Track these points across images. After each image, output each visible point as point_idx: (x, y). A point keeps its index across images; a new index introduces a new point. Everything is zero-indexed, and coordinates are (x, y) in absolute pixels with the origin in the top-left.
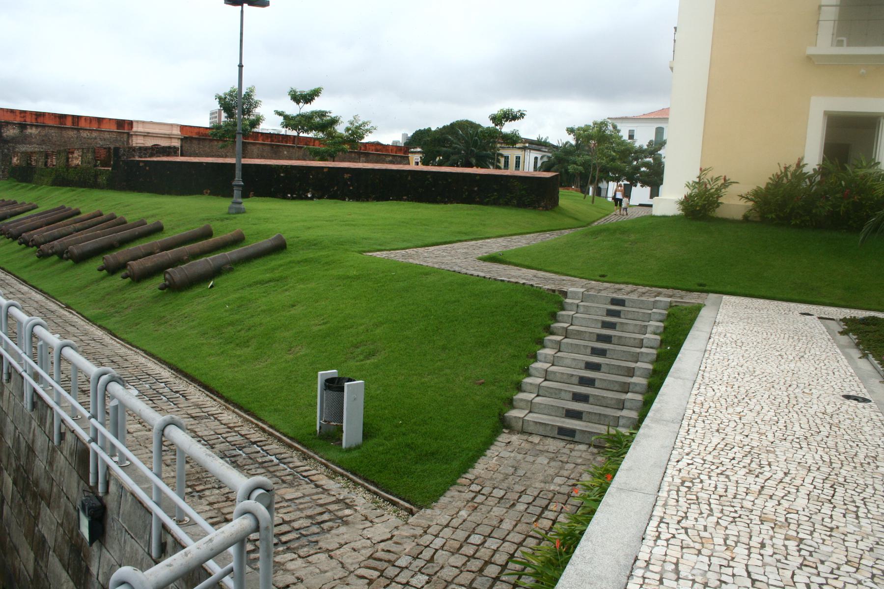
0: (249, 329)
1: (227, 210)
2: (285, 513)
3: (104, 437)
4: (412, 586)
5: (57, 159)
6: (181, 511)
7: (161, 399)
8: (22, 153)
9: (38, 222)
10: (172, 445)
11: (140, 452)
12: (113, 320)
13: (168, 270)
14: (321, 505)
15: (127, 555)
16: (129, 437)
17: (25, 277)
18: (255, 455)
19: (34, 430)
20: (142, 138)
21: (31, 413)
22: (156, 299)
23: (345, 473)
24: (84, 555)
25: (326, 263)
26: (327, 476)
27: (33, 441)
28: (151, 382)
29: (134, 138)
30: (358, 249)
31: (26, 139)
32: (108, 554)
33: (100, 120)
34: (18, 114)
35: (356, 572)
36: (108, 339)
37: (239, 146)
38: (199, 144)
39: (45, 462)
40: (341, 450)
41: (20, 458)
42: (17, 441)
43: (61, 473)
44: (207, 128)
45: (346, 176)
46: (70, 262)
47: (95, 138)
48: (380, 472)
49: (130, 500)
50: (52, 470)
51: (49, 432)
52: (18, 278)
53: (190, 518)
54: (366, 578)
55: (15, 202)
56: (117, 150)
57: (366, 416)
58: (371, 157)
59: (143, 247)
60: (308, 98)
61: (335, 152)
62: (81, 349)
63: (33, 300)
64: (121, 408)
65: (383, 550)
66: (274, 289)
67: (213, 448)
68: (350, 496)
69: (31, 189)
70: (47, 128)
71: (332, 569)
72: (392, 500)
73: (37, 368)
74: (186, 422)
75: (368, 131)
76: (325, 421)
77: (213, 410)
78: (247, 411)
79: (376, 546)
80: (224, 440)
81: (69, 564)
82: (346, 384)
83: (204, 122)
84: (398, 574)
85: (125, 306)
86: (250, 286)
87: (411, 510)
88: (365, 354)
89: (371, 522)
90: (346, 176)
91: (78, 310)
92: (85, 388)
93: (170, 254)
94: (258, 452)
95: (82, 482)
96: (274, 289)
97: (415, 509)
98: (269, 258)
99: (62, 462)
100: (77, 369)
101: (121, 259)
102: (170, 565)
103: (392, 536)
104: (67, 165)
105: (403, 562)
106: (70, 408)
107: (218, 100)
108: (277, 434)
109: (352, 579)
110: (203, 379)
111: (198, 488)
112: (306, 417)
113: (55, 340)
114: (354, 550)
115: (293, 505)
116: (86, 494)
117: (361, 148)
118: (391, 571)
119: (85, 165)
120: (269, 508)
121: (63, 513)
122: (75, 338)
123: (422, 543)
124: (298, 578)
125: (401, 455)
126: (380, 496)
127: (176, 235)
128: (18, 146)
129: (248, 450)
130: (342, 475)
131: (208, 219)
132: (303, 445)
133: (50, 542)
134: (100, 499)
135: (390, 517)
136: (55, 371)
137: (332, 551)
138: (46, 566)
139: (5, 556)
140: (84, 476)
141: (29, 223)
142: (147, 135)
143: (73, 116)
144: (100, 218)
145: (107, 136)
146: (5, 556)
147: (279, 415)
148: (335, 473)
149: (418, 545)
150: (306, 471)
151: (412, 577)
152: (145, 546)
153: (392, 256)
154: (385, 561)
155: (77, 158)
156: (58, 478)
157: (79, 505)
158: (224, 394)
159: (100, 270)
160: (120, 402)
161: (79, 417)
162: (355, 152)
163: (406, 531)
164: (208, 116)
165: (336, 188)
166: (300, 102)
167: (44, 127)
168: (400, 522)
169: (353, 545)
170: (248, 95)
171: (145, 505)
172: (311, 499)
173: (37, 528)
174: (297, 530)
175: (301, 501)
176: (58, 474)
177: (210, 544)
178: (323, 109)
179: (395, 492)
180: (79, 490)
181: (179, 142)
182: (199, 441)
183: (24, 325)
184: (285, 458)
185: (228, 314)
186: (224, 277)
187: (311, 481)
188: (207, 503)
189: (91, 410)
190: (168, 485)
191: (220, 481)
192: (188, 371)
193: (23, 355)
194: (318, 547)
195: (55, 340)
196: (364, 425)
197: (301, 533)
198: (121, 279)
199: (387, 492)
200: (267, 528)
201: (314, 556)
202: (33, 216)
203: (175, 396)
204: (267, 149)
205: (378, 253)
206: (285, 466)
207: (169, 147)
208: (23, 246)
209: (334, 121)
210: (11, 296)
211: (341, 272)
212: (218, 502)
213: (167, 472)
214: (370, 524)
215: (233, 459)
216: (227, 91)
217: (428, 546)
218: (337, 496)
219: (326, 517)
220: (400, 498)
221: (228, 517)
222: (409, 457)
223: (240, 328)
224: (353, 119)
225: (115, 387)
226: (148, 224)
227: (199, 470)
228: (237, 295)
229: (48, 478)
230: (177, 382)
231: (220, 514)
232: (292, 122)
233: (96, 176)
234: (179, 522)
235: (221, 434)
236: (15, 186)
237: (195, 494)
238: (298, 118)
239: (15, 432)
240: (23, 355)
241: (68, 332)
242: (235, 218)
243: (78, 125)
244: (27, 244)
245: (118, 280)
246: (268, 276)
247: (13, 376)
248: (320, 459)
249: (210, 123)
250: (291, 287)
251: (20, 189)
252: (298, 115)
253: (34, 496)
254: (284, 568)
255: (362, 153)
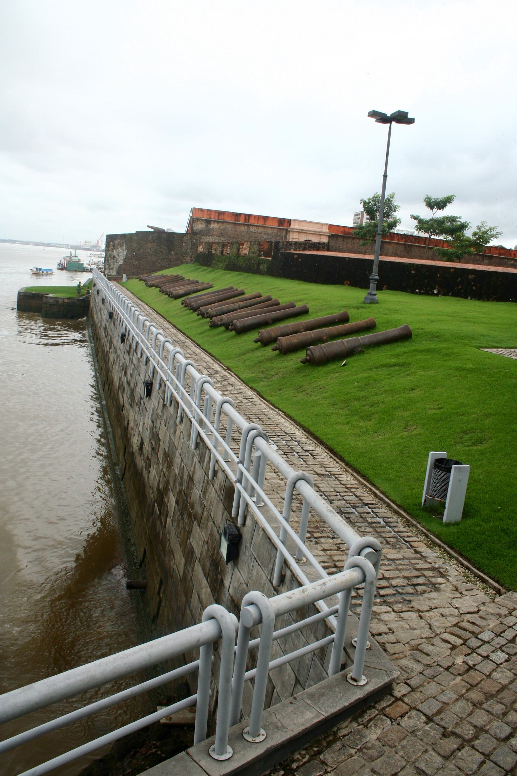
0: (372, 405)
1: (363, 300)
2: (386, 570)
3: (247, 480)
4: (491, 660)
5: (231, 249)
6: (300, 551)
7: (294, 455)
8: (206, 243)
9: (212, 299)
10: (299, 495)
11: (272, 496)
12: (262, 384)
13: (309, 347)
14: (417, 570)
15: (254, 578)
16: (266, 482)
17: (199, 342)
18: (366, 515)
19: (195, 464)
20: (297, 234)
21: (195, 451)
22: (298, 370)
23: (442, 545)
24: (221, 570)
25: (446, 354)
26: (425, 544)
27: (194, 472)
28: (287, 439)
29: (291, 234)
30: (476, 344)
31: (209, 232)
32: (239, 573)
33: (265, 218)
34: (206, 212)
35: (441, 636)
36: (256, 399)
37: (377, 245)
38: (343, 241)
39: (200, 491)
40: (441, 524)
41: (182, 484)
42: (182, 470)
43: (211, 502)
44: (351, 228)
45: (471, 277)
46: (234, 333)
47: (261, 233)
48: (474, 549)
49: (261, 535)
50: (205, 499)
51: (206, 468)
52: (194, 342)
53: (307, 559)
54: (450, 643)
55: (197, 282)
56: (277, 243)
57: (468, 497)
58: (494, 260)
59: (291, 325)
60: (441, 204)
61: (461, 254)
62: (235, 405)
63: (204, 361)
64: (263, 459)
65: (468, 621)
66: (398, 373)
67: (331, 503)
68: (444, 566)
69: (209, 272)
70: (225, 224)
71: (421, 628)
72: (483, 578)
73: (203, 416)
74: (313, 478)
75: (495, 236)
76: (430, 496)
77: (336, 471)
78: (363, 476)
79: (463, 616)
80: (341, 498)
81: (209, 574)
82: (454, 466)
83: (349, 222)
84: (480, 646)
85: (273, 373)
86: (377, 368)
87: (499, 590)
88: (473, 441)
89: (461, 593)
90: (471, 277)
91: (236, 373)
92: (236, 436)
93: (312, 334)
94: (369, 513)
95: (226, 513)
96: (398, 373)
97: (502, 590)
98: (395, 345)
99: (212, 493)
100: (232, 421)
101: (273, 334)
102: (290, 598)
103: (479, 611)
104: (238, 255)
105: (486, 636)
106: (224, 452)
107: (362, 204)
108: (387, 500)
109: (437, 641)
110: (329, 443)
111: (316, 535)
112: (413, 489)
113: (218, 396)
114: (443, 616)
115: (393, 564)
116: (228, 523)
117: (485, 251)
118: (473, 642)
119: (251, 254)
120: (375, 565)
121: (209, 534)
122: (232, 395)
123: (506, 623)
124: (390, 629)
125: (496, 537)
126: (472, 572)
127: (319, 318)
128: (203, 237)
129: (360, 510)
130: (440, 546)
131: (346, 307)
132: (408, 514)
133: (197, 554)
134: (238, 529)
135: (478, 592)
136: (216, 420)
137: (422, 612)
138: (193, 572)
139: (165, 557)
140: (228, 507)
141: (206, 299)
142: (301, 232)
143: (246, 215)
144: (259, 299)
145: (270, 231)
146: (165, 557)
147: (390, 484)
148: (433, 542)
149: (502, 624)
150: (408, 537)
151: (493, 652)
152: (268, 574)
153: (507, 353)
154: (470, 632)
155: (245, 249)
156: (208, 505)
157: (222, 530)
158: (346, 459)
159: (256, 341)
160: (263, 454)
161: (230, 460)
162: (480, 255)
163: (491, 609)
164: (353, 218)
165: (460, 287)
166: (434, 208)
167: (223, 222)
168: (487, 599)
169: (441, 610)
170: (389, 200)
171: (272, 541)
172: (410, 562)
173: (189, 541)
174: (395, 587)
175: (401, 562)
176: (209, 502)
177: (324, 587)
178: (454, 215)
179: (486, 571)
180: (223, 518)
181: (327, 238)
182: (321, 495)
183: (196, 381)
184: (391, 522)
185: (356, 390)
186: (355, 358)
187: (412, 546)
188: (322, 549)
189: (240, 456)
190: (292, 527)
191: (334, 532)
192: (318, 434)
193: (194, 405)
194: (410, 606)
195: (218, 396)
196: (465, 504)
197: (397, 591)
198: (271, 351)
199: (478, 569)
200: (372, 583)
201: (406, 613)
202: (207, 294)
203: (305, 454)
204: (401, 248)
205: (494, 349)
206: (390, 529)
207: (319, 243)
208: (200, 316)
209: (463, 226)
210: (188, 356)
211: (458, 364)
212: (331, 550)
213: (294, 517)
214: (459, 595)
215: (347, 516)
216: (371, 196)
217: (511, 627)
218: (433, 564)
219: (421, 580)
220: (490, 577)
221: (338, 564)
222: (503, 541)
223: (365, 403)
224: (480, 225)
225: (260, 441)
226: (297, 307)
227: (318, 519)
228: (365, 375)
229: (201, 504)
230: (308, 442)
231: (331, 560)
232: (425, 226)
233: (259, 264)
234: (298, 560)
235: (339, 492)
236: (197, 269)
237: (312, 539)
238: (431, 222)
239: (181, 463)
240: (194, 405)
241: (227, 390)
242: (369, 307)
243: (248, 222)
244: (203, 315)
245: (269, 352)
246: (394, 360)
247: (184, 420)
248: (422, 528)
249: (354, 223)
250: (412, 373)
251: (202, 271)
252: (431, 220)
253: (190, 516)
254: (379, 617)
255: (486, 256)
